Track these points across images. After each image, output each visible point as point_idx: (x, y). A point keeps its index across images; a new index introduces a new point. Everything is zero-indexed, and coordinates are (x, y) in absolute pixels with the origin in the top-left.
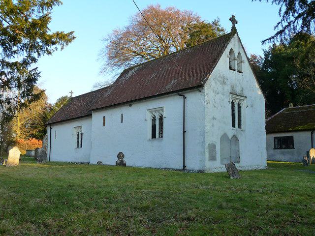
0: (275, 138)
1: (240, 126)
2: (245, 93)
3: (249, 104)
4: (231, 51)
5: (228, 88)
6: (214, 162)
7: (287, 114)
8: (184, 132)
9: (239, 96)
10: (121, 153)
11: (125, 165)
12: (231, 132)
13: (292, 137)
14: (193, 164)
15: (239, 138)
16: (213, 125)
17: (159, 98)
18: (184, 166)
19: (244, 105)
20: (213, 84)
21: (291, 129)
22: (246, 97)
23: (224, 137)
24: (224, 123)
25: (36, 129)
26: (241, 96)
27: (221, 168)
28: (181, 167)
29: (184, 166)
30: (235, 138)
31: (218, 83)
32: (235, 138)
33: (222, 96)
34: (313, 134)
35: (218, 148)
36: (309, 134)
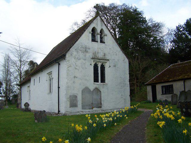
0: (162, 87)
1: (103, 80)
2: (108, 57)
3: (112, 65)
4: (94, 30)
5: (90, 55)
6: (76, 108)
7: (173, 68)
8: (59, 87)
9: (102, 59)
10: (27, 103)
11: (30, 111)
12: (92, 85)
13: (173, 85)
14: (63, 111)
15: (101, 90)
16: (74, 82)
17: (52, 65)
18: (59, 111)
19: (107, 66)
20: (75, 53)
21: (171, 80)
22: (108, 60)
23: (86, 90)
24: (86, 80)
25: (133, 83)
26: (103, 60)
27: (82, 112)
28: (57, 112)
29: (59, 111)
30: (97, 90)
31: (80, 52)
32: (97, 90)
33: (84, 62)
34: (185, 83)
35: (80, 98)
36: (182, 83)
